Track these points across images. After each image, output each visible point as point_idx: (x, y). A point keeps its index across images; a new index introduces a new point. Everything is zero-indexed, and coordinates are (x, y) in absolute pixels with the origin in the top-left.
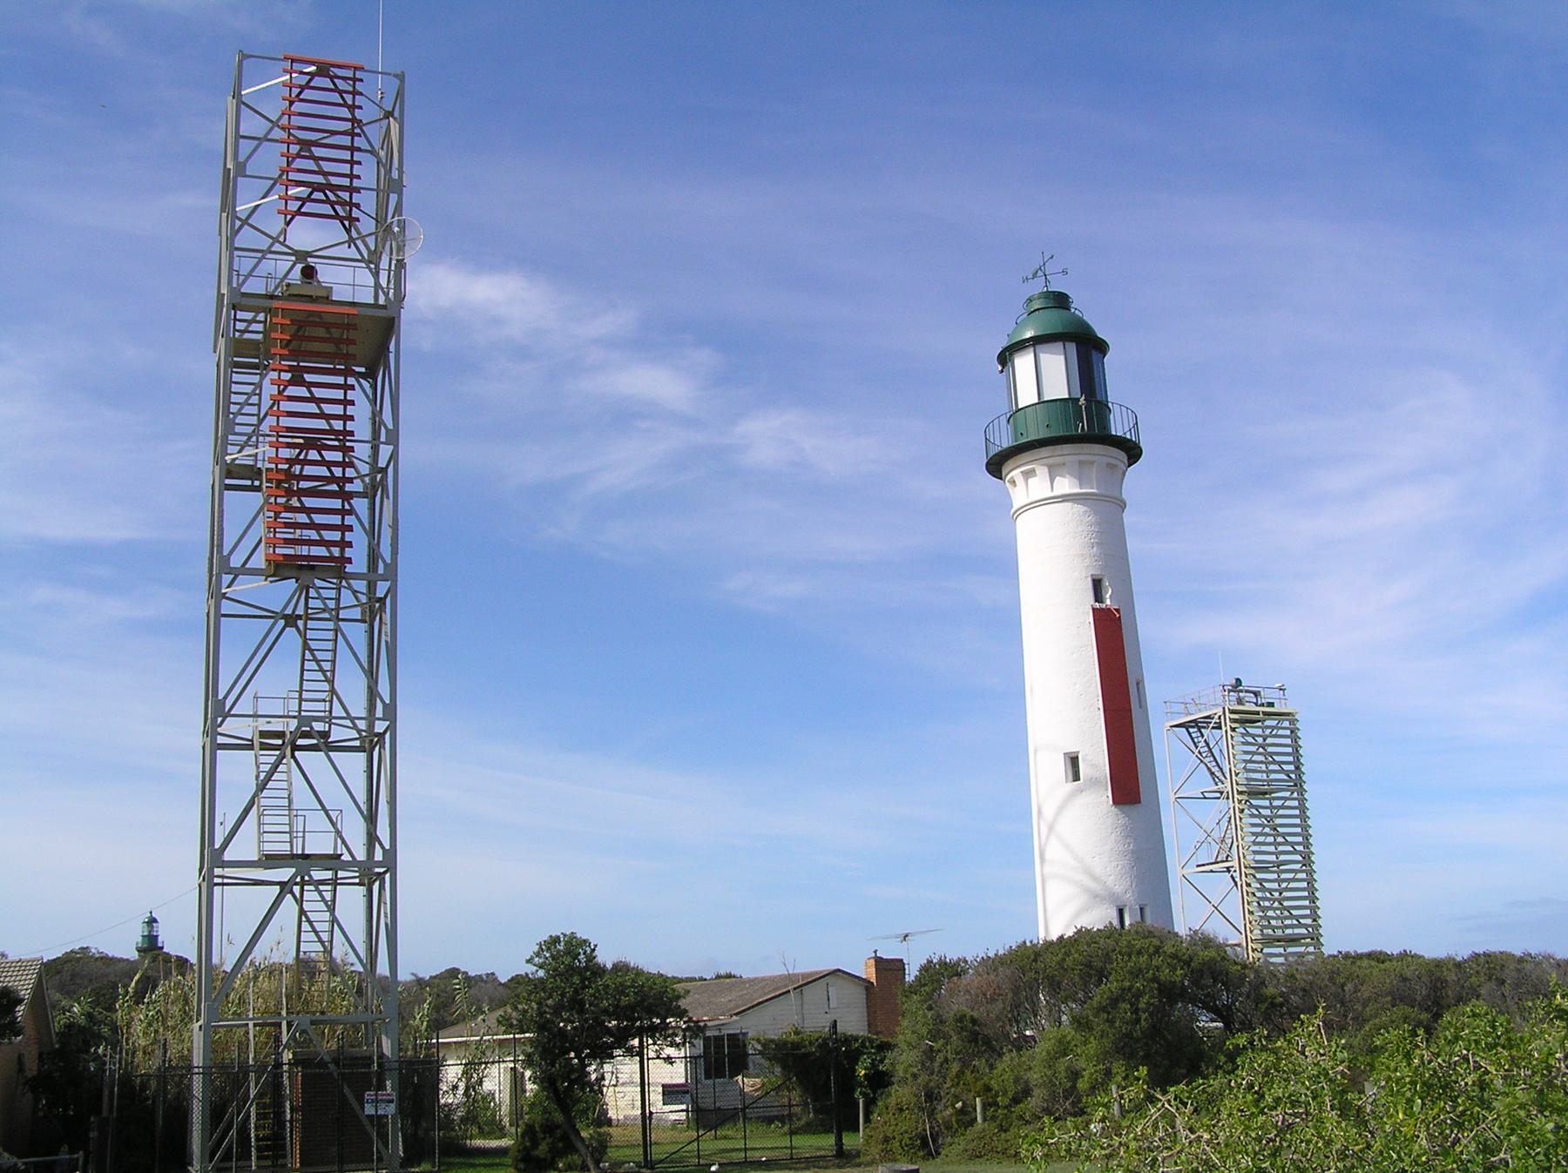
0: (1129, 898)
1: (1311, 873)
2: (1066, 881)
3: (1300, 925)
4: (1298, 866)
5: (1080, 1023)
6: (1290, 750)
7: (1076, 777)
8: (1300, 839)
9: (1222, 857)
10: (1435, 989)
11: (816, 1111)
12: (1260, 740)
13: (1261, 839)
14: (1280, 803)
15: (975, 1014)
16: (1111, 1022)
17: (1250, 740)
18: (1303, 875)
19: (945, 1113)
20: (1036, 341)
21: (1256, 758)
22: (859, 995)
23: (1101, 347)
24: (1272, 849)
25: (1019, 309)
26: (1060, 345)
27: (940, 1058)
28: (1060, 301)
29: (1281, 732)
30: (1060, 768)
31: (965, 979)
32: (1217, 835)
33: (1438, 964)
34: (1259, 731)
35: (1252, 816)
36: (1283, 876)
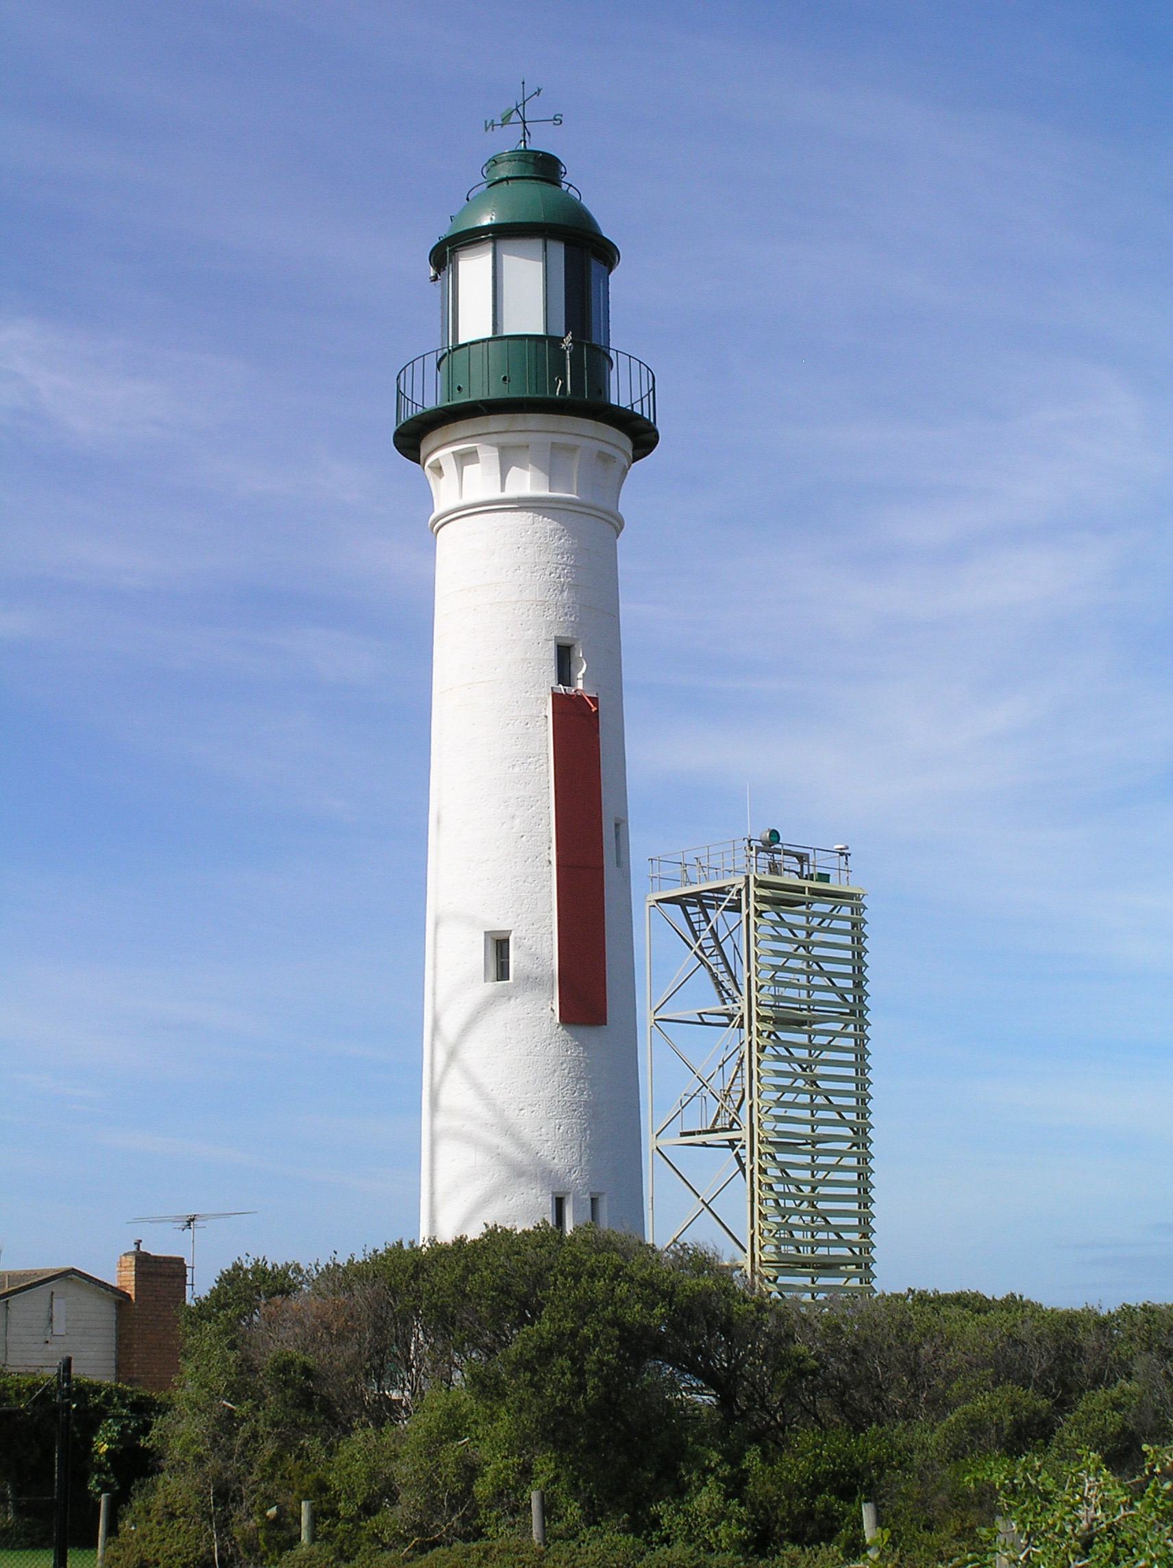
0: (576, 1182)
1: (865, 1158)
2: (470, 1144)
3: (840, 1242)
4: (845, 1146)
5: (487, 1387)
6: (848, 955)
7: (502, 973)
8: (852, 1102)
9: (724, 1122)
10: (1061, 1359)
11: (19, 1510)
12: (802, 935)
13: (788, 1097)
14: (823, 1040)
15: (311, 1361)
16: (538, 1388)
17: (785, 932)
18: (852, 1162)
19: (247, 1524)
20: (501, 233)
21: (793, 963)
22: (103, 1315)
23: (607, 254)
24: (806, 1114)
25: (476, 177)
26: (536, 245)
27: (244, 1431)
28: (546, 168)
29: (836, 924)
30: (477, 954)
31: (295, 1302)
32: (717, 1085)
33: (1072, 1320)
34: (801, 921)
35: (778, 1058)
36: (821, 1160)
